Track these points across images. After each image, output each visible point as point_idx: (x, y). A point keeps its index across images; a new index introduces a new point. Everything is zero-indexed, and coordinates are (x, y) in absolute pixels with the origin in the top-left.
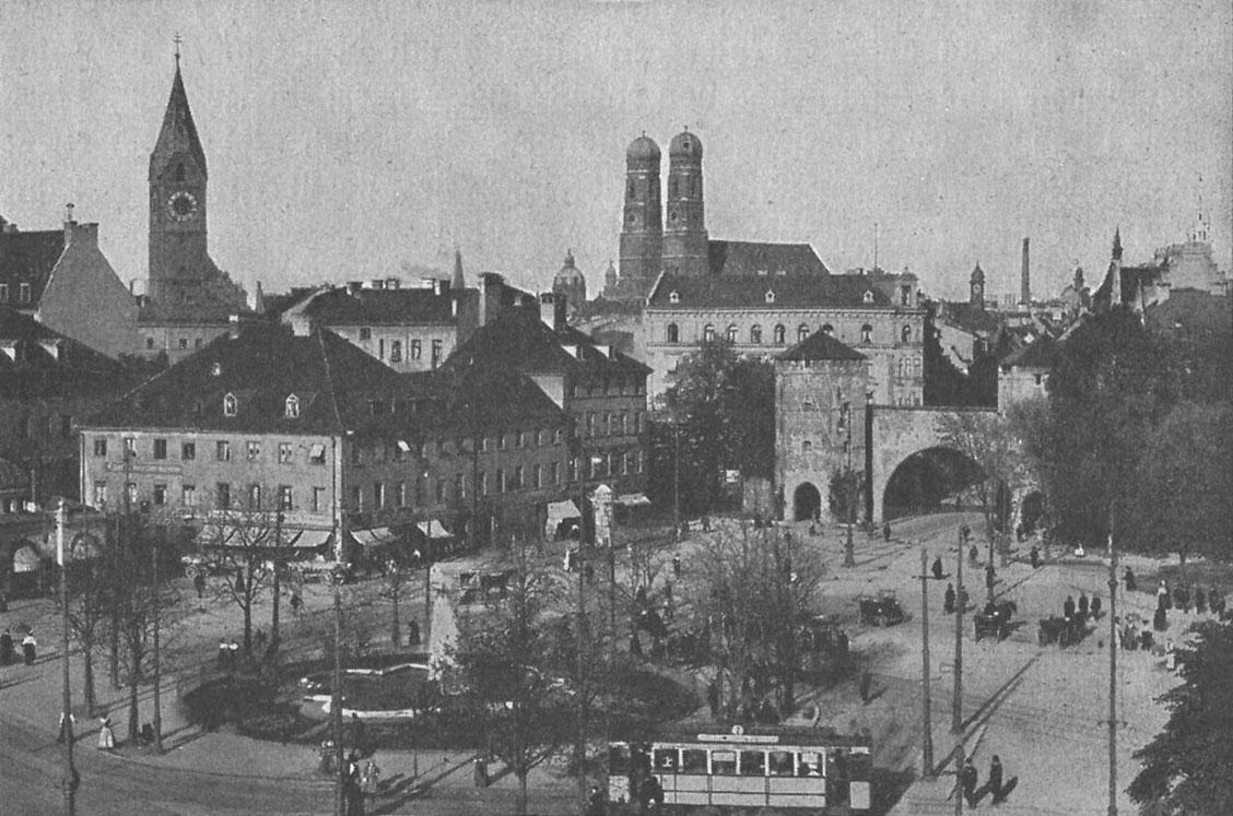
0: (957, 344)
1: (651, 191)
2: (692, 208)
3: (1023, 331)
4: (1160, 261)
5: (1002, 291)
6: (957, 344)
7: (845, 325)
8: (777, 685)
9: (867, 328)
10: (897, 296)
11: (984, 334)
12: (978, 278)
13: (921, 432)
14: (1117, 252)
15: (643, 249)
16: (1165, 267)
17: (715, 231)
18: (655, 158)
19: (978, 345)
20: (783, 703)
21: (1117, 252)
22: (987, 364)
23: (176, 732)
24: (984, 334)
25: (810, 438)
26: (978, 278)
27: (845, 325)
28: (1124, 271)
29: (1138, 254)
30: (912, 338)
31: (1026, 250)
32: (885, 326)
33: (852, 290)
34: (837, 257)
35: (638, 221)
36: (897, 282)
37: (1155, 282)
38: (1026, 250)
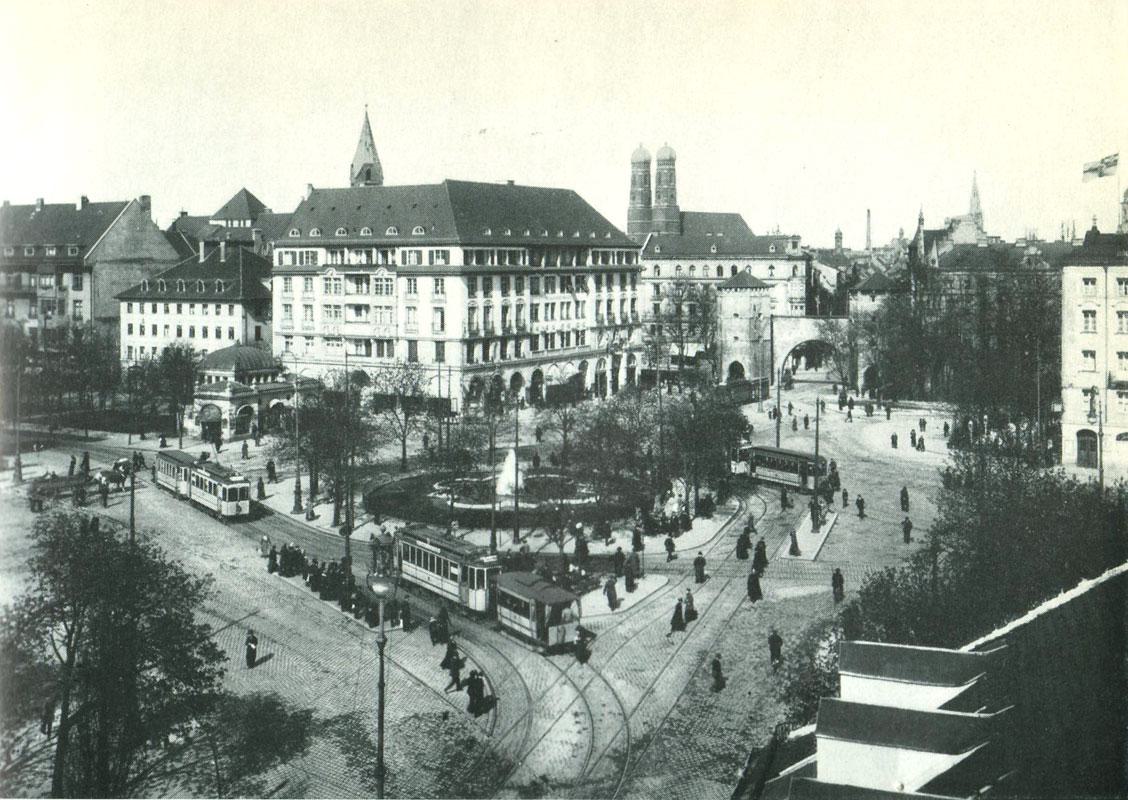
0: (829, 277)
1: (645, 183)
2: (671, 195)
3: (866, 266)
4: (948, 226)
5: (854, 244)
6: (829, 277)
7: (759, 269)
8: (915, 313)
9: (772, 267)
10: (789, 250)
11: (842, 268)
12: (839, 237)
13: (807, 330)
14: (921, 221)
15: (644, 213)
16: (951, 229)
17: (685, 204)
18: (647, 163)
19: (839, 275)
20: (600, 574)
21: (921, 221)
22: (849, 285)
23: (523, 626)
24: (842, 268)
25: (738, 335)
26: (839, 237)
27: (759, 269)
28: (925, 232)
29: (934, 224)
30: (798, 273)
31: (869, 215)
32: (783, 268)
33: (762, 248)
34: (759, 228)
35: (638, 200)
36: (790, 240)
37: (945, 238)
38: (869, 215)
